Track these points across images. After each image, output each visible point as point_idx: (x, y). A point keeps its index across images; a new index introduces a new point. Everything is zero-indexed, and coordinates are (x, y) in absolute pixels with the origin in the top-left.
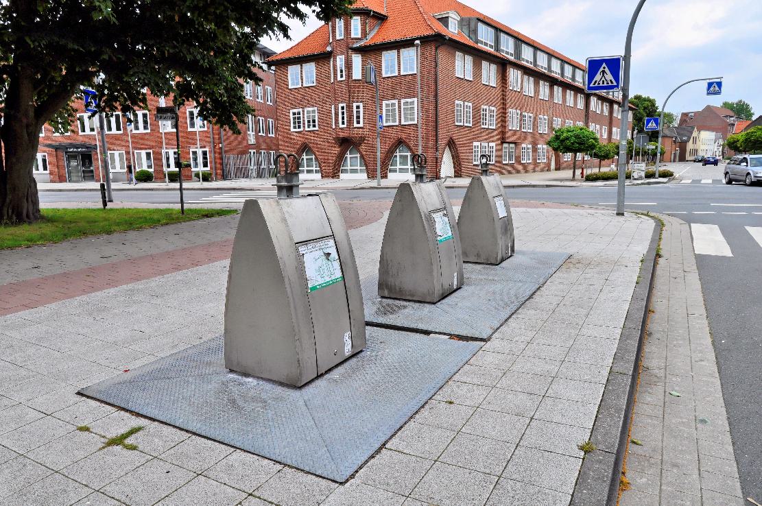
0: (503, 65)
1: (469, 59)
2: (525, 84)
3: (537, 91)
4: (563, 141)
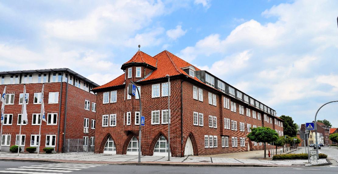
0: (220, 95)
1: (201, 91)
3: (238, 110)
4: (257, 136)
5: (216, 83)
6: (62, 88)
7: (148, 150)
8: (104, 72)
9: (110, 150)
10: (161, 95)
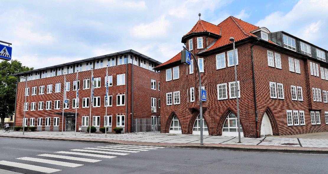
0: (304, 59)
2: (322, 73)
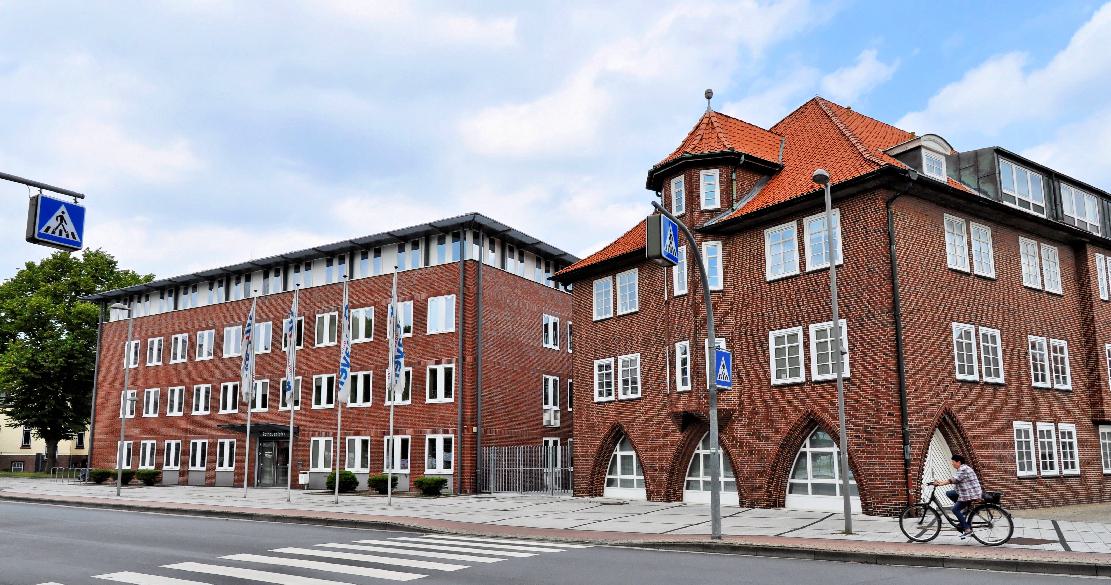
5: (1054, 200)
6: (466, 282)
7: (766, 488)
8: (596, 215)
9: (626, 484)
10: (803, 264)
